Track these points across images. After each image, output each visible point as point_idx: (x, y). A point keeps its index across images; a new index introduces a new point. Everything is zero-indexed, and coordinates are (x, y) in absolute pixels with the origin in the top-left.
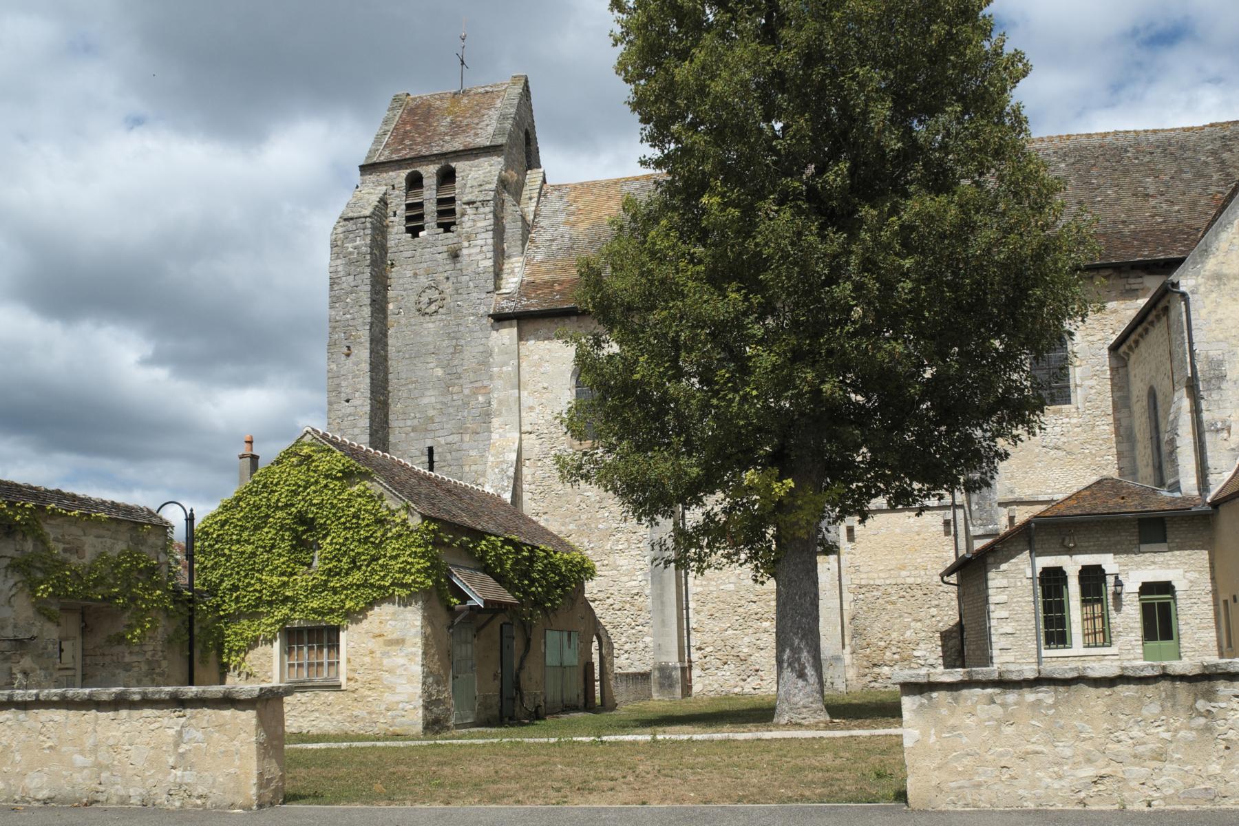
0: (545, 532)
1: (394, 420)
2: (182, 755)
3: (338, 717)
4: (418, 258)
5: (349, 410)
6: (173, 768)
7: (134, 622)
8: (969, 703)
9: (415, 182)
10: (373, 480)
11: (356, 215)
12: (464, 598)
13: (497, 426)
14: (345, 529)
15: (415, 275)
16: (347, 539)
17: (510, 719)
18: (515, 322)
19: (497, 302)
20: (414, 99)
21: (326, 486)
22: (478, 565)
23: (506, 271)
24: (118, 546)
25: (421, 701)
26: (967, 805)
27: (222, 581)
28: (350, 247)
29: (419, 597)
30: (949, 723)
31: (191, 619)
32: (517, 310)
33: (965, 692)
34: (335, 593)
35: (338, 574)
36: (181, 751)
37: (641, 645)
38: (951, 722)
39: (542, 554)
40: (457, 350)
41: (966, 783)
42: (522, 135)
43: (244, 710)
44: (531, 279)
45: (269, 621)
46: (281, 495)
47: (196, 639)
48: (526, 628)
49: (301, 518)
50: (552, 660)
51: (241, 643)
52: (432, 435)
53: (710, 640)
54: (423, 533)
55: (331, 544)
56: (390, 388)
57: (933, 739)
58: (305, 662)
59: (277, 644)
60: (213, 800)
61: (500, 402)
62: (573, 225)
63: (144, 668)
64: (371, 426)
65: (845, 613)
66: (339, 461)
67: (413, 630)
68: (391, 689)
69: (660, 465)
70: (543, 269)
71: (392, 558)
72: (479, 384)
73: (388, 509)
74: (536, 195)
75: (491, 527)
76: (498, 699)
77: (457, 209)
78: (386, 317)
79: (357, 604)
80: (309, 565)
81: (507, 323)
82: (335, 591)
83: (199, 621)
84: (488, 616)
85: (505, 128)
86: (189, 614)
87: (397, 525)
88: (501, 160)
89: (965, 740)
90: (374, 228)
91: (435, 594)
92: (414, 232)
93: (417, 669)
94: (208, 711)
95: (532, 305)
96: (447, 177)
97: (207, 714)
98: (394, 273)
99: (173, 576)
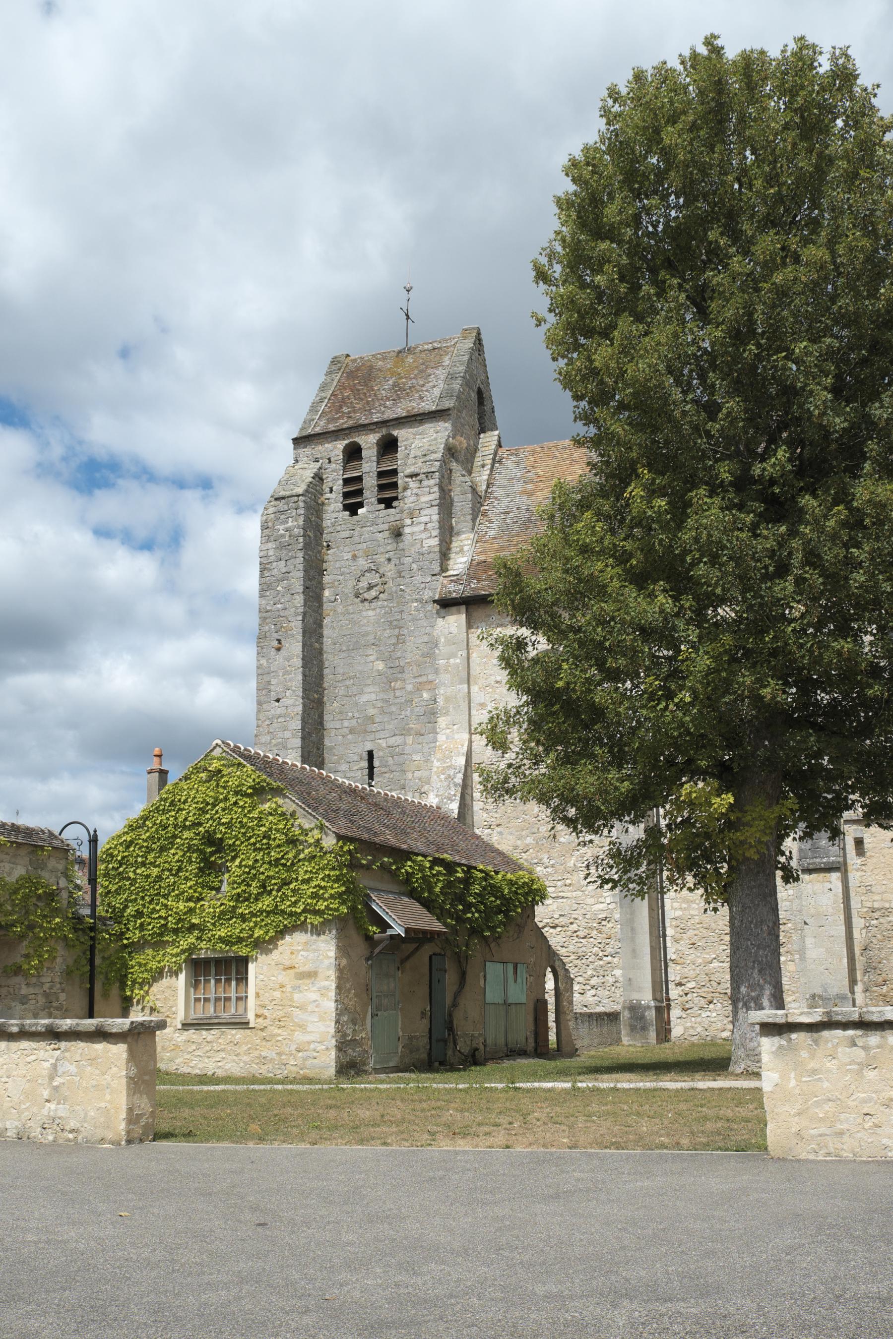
0: (489, 849)
1: (330, 722)
2: (56, 1088)
3: (246, 1058)
4: (356, 539)
5: (279, 711)
6: (48, 1101)
7: (32, 952)
8: (830, 1045)
9: (353, 453)
10: (285, 797)
11: (288, 493)
12: (384, 926)
13: (443, 726)
14: (255, 850)
15: (354, 557)
16: (256, 861)
17: (442, 1063)
18: (463, 608)
19: (444, 586)
20: (354, 361)
21: (236, 803)
22: (403, 889)
23: (454, 550)
24: (15, 871)
25: (334, 1042)
26: (829, 1154)
27: (126, 907)
28: (281, 528)
29: (333, 926)
30: (809, 1067)
31: (92, 948)
32: (466, 594)
33: (826, 1034)
34: (244, 921)
35: (247, 899)
36: (55, 1084)
37: (611, 980)
38: (812, 1065)
39: (480, 875)
40: (400, 640)
41: (828, 1131)
42: (474, 395)
43: (116, 1044)
44: (482, 558)
45: (174, 952)
46: (189, 812)
47: (98, 970)
48: (462, 961)
49: (209, 839)
50: (493, 995)
51: (145, 975)
52: (372, 737)
53: (692, 974)
54: (337, 854)
55: (240, 866)
56: (325, 685)
57: (793, 1083)
58: (212, 996)
59: (182, 976)
60: (84, 1134)
61: (447, 700)
62: (530, 494)
63: (42, 1000)
64: (303, 729)
65: (856, 942)
66: (249, 776)
67: (326, 962)
68: (302, 1027)
69: (587, 780)
70: (496, 546)
71: (304, 882)
72: (424, 679)
73: (301, 828)
74: (490, 462)
75: (420, 846)
76: (426, 1040)
77: (400, 482)
78: (321, 605)
79: (267, 933)
80: (218, 890)
81: (454, 609)
82: (243, 918)
83: (101, 951)
84: (414, 946)
85: (453, 390)
86: (90, 943)
87: (310, 845)
88: (448, 425)
89: (826, 1084)
90: (307, 507)
91: (351, 922)
92: (352, 509)
93: (330, 1005)
94: (81, 1044)
95: (483, 589)
96: (389, 446)
97: (80, 1048)
98: (330, 556)
99: (73, 903)
